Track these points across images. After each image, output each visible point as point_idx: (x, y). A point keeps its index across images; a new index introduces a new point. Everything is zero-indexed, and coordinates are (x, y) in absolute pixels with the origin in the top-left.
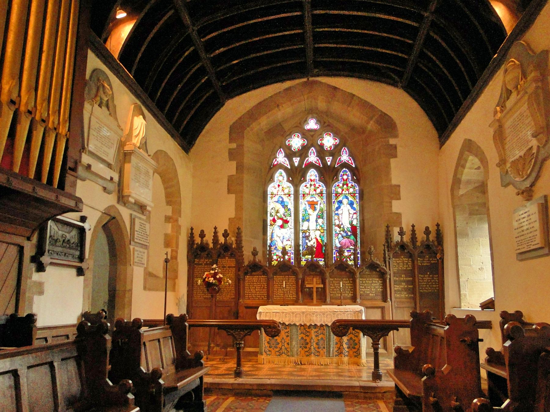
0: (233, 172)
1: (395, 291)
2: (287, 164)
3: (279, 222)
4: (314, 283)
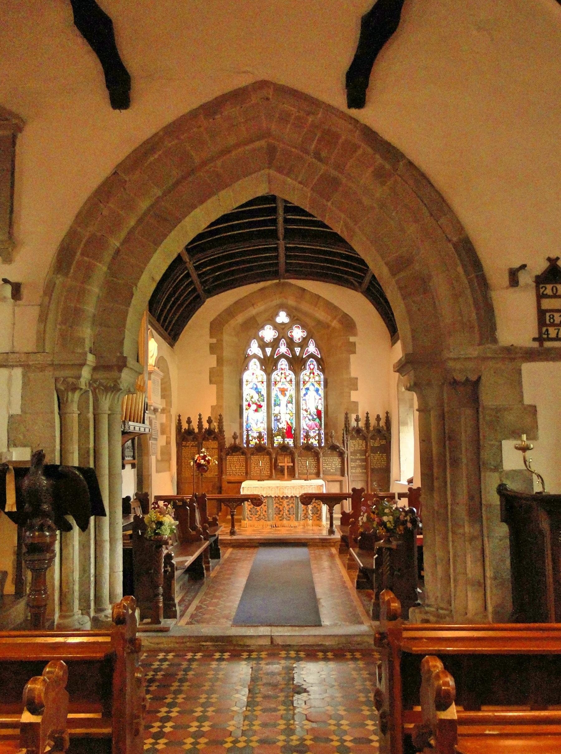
0: (214, 364)
1: (352, 467)
2: (260, 354)
3: (254, 407)
4: (285, 462)
